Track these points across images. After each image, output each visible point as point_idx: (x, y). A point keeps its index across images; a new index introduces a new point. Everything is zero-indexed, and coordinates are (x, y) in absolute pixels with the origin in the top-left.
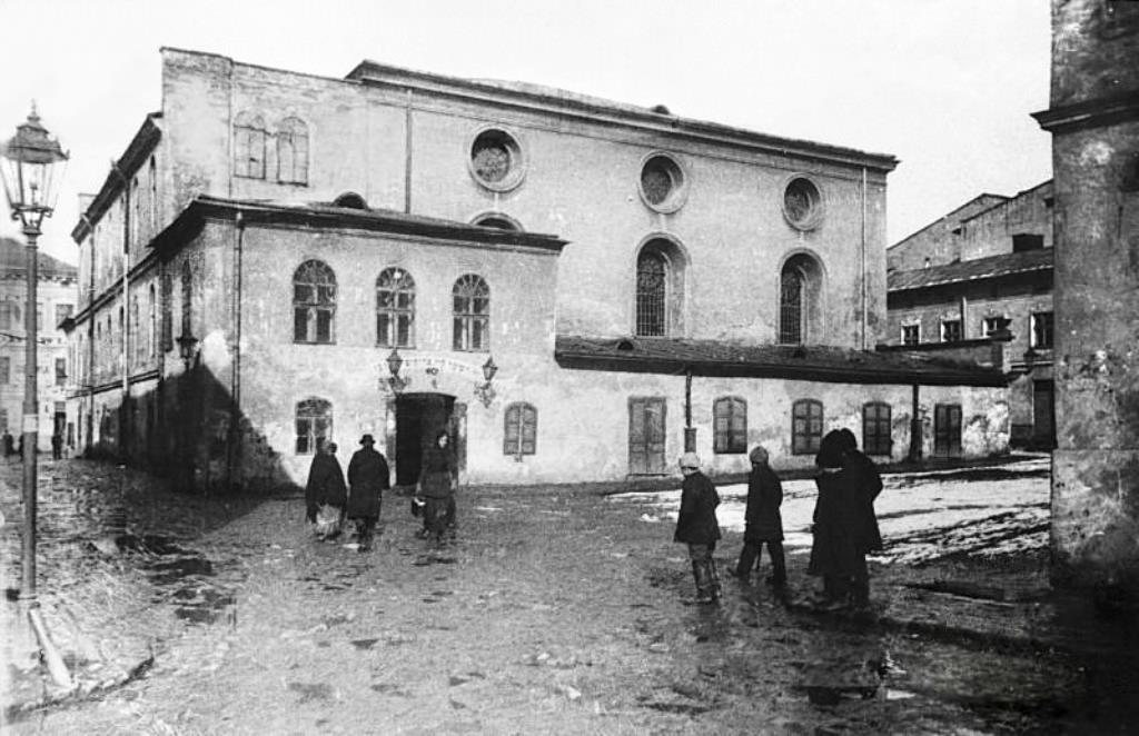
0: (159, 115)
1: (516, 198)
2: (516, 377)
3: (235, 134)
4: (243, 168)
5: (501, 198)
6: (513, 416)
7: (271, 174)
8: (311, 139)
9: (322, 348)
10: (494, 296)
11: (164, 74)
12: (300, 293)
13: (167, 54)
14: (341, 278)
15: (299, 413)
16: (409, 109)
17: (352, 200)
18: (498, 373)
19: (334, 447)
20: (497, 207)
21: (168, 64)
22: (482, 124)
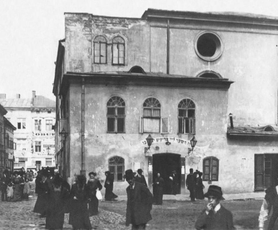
0: (64, 41)
1: (219, 63)
2: (209, 145)
3: (94, 45)
4: (97, 60)
5: (211, 64)
6: (207, 163)
7: (109, 61)
8: (126, 45)
9: (120, 135)
10: (197, 108)
11: (65, 24)
12: (110, 111)
13: (67, 15)
14: (127, 103)
15: (110, 163)
16: (168, 28)
17: (137, 69)
18: (197, 144)
19: (35, 165)
20: (209, 68)
21: (66, 20)
22: (202, 31)
